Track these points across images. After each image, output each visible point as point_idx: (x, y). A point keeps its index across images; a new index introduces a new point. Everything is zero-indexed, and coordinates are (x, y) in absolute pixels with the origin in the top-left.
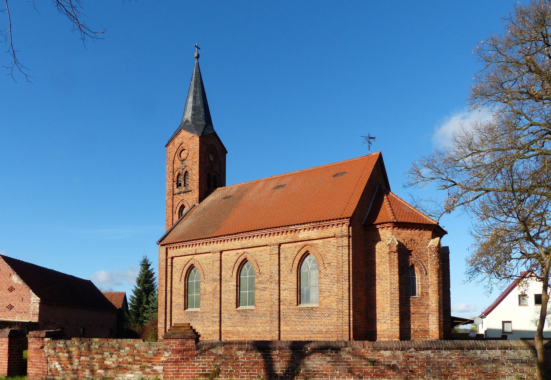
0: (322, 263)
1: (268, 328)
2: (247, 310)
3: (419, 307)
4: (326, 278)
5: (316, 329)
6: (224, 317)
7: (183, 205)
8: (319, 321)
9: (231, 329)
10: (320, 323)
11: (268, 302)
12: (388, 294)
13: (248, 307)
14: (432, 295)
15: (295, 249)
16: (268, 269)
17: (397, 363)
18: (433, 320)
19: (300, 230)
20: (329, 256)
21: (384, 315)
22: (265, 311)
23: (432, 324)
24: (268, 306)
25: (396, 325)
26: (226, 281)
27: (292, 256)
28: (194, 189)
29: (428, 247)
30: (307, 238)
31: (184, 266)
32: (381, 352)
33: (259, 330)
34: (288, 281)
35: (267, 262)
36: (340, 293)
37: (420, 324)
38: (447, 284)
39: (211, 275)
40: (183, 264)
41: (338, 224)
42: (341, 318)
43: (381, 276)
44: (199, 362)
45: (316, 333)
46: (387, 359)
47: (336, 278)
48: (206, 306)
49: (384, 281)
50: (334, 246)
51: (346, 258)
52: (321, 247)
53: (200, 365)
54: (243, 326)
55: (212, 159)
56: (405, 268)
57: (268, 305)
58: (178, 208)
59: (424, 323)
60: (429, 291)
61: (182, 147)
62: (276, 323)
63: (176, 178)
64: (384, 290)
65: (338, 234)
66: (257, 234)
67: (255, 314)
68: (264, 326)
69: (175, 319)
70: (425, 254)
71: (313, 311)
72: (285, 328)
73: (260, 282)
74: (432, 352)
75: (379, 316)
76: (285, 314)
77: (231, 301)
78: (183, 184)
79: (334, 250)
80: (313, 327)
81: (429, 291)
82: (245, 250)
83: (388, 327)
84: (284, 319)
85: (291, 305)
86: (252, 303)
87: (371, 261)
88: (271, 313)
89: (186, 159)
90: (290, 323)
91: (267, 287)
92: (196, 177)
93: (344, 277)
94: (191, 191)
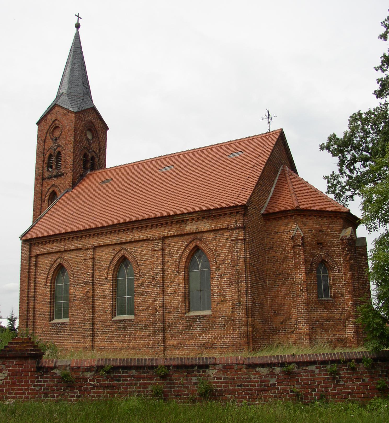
0: (214, 261)
1: (151, 342)
2: (124, 320)
3: (332, 311)
4: (219, 279)
5: (209, 342)
6: (98, 330)
7: (54, 191)
8: (212, 333)
9: (106, 344)
10: (213, 334)
11: (150, 310)
12: (295, 297)
13: (126, 317)
14: (347, 297)
15: (181, 243)
16: (150, 268)
17: (276, 381)
18: (350, 327)
19: (187, 220)
20: (221, 251)
21: (291, 323)
22: (147, 321)
23: (349, 332)
24: (151, 315)
25: (305, 335)
26: (100, 284)
27: (179, 253)
28: (67, 172)
29: (340, 238)
30: (195, 230)
31: (50, 265)
32: (257, 370)
33: (140, 345)
34: (174, 284)
35: (149, 260)
36: (236, 297)
37: (335, 333)
38: (366, 282)
39: (82, 277)
40: (50, 263)
41: (231, 213)
42: (238, 327)
43: (286, 275)
44: (40, 385)
45: (209, 348)
46: (264, 378)
47: (231, 278)
48: (76, 316)
49: (289, 280)
50: (228, 239)
51: (241, 254)
52: (213, 241)
53: (41, 389)
54: (121, 341)
55: (90, 137)
56: (314, 265)
57: (150, 313)
58: (48, 194)
59: (340, 331)
60: (343, 291)
61: (56, 124)
62: (160, 336)
63: (46, 159)
64: (291, 292)
65: (231, 225)
66: (136, 226)
67: (134, 325)
68: (146, 340)
69: (39, 332)
70: (336, 248)
71: (204, 320)
72: (171, 342)
73: (141, 285)
74: (317, 368)
75: (286, 325)
76: (171, 325)
77: (106, 309)
78: (54, 166)
79: (227, 244)
80: (205, 340)
81: (344, 292)
82: (123, 246)
83: (297, 337)
84: (169, 331)
85: (178, 313)
86: (131, 312)
87: (274, 257)
88: (154, 323)
89: (59, 138)
90: (177, 336)
91: (149, 291)
92: (70, 159)
93: (240, 277)
94: (63, 175)
